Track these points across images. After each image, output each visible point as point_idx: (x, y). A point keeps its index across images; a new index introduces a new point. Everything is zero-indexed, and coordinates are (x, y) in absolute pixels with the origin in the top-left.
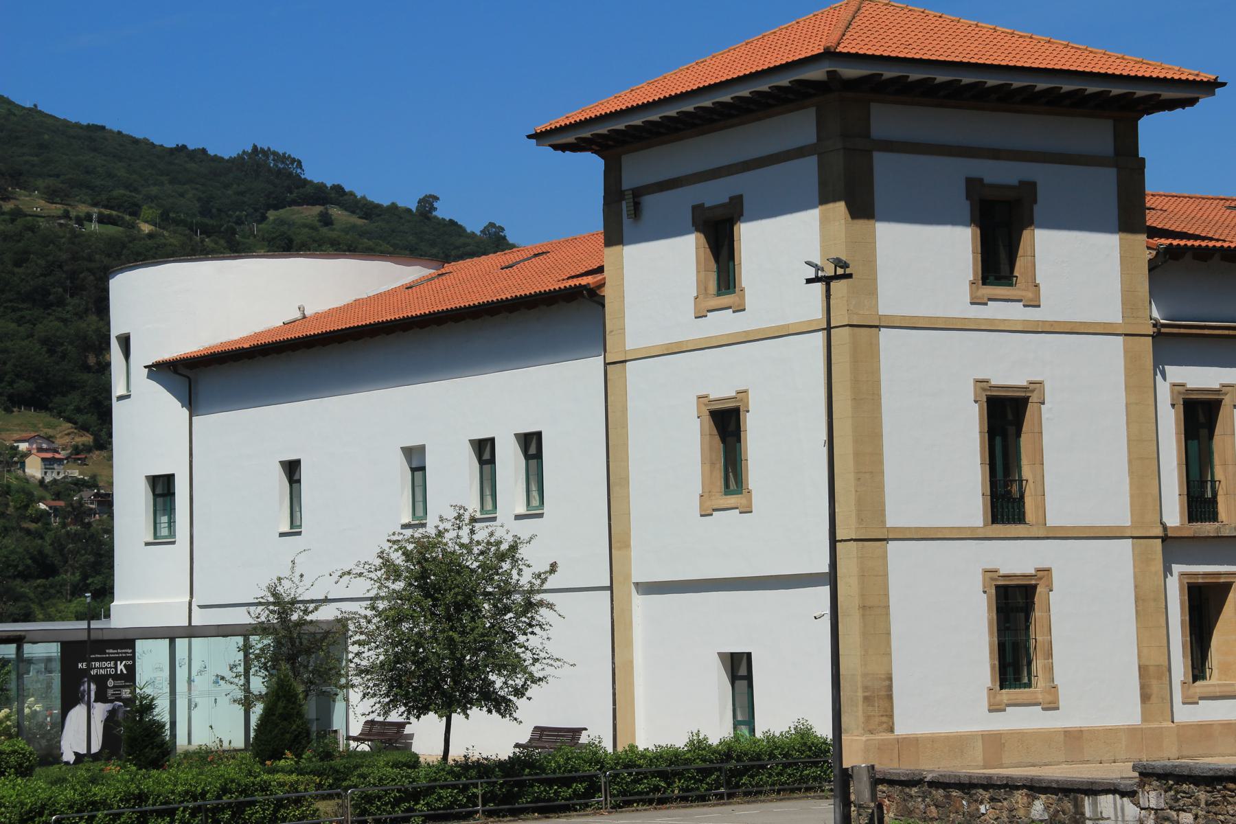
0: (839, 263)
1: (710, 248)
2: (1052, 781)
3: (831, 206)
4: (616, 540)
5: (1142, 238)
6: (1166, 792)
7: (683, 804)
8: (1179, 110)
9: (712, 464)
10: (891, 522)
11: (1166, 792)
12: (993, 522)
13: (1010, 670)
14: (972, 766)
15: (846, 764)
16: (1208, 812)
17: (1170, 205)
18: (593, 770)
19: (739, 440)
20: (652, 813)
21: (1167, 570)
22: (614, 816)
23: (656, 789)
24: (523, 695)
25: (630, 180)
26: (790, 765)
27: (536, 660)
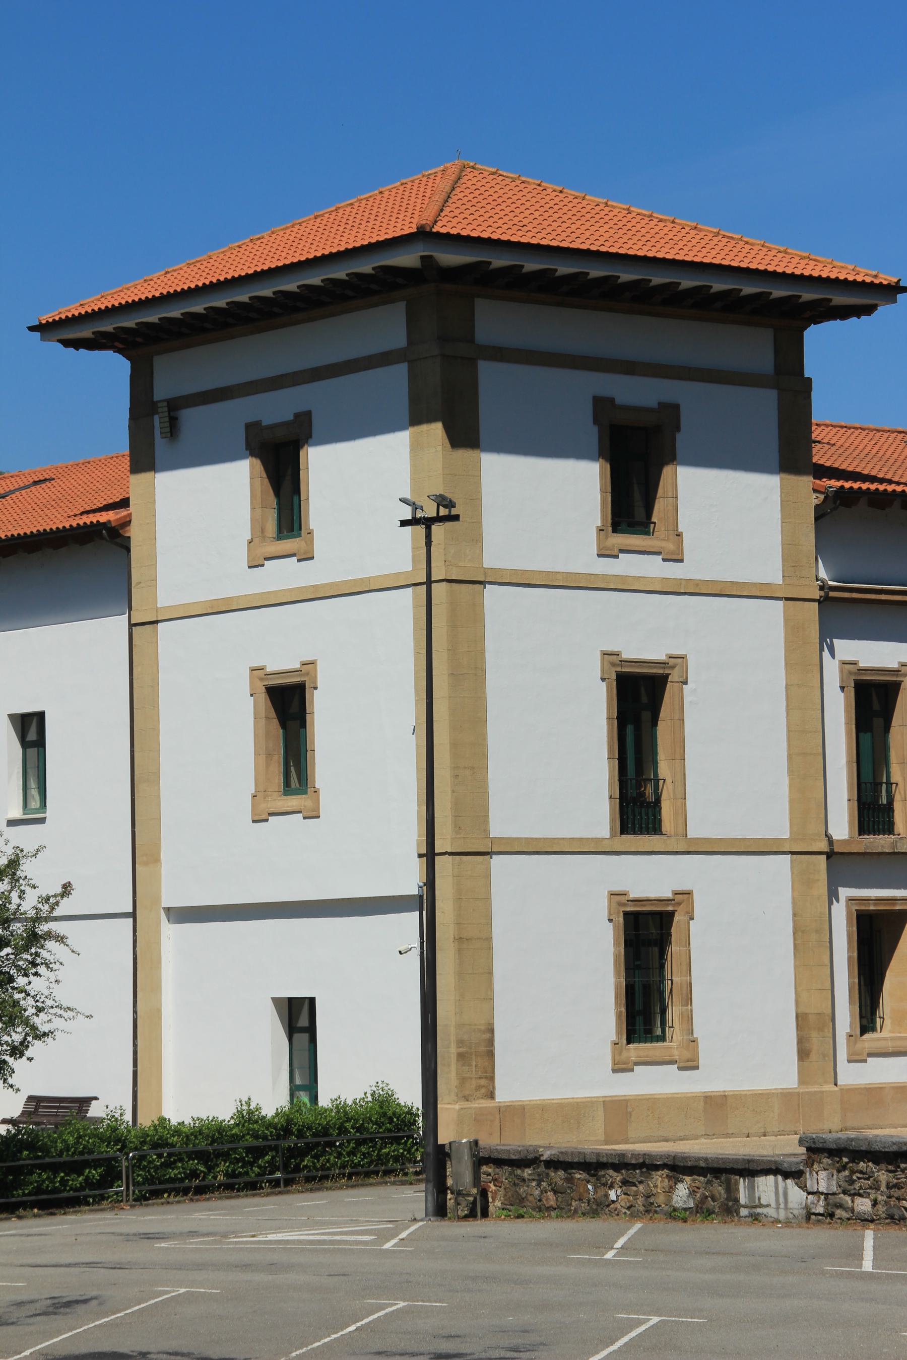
0: (443, 501)
1: (269, 477)
2: (699, 1159)
3: (424, 427)
4: (142, 853)
5: (806, 482)
6: (839, 1171)
7: (228, 1193)
8: (854, 320)
9: (269, 755)
10: (497, 829)
11: (839, 1171)
12: (622, 833)
13: (639, 1020)
14: (592, 1140)
15: (444, 1138)
16: (890, 1197)
17: (838, 437)
18: (111, 1151)
19: (303, 724)
20: (187, 1206)
21: (833, 895)
22: (139, 1210)
23: (194, 1174)
24: (22, 1055)
25: (163, 390)
26: (363, 1142)
27: (40, 1010)
